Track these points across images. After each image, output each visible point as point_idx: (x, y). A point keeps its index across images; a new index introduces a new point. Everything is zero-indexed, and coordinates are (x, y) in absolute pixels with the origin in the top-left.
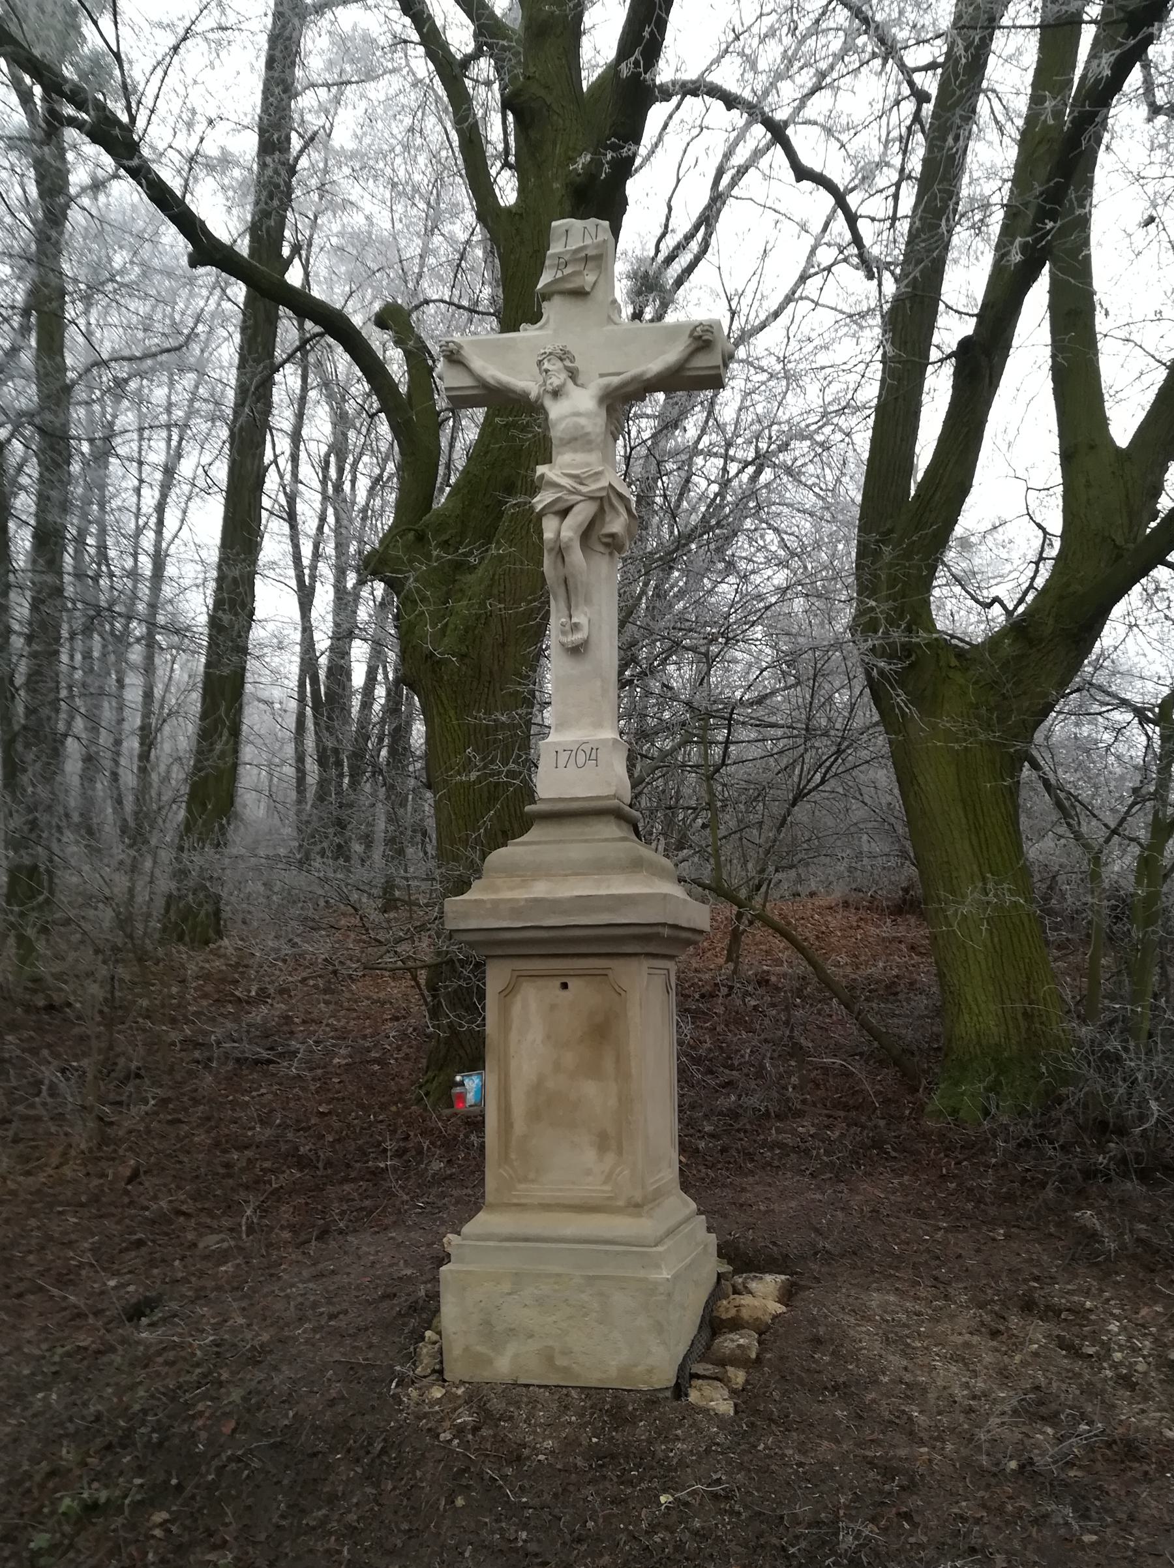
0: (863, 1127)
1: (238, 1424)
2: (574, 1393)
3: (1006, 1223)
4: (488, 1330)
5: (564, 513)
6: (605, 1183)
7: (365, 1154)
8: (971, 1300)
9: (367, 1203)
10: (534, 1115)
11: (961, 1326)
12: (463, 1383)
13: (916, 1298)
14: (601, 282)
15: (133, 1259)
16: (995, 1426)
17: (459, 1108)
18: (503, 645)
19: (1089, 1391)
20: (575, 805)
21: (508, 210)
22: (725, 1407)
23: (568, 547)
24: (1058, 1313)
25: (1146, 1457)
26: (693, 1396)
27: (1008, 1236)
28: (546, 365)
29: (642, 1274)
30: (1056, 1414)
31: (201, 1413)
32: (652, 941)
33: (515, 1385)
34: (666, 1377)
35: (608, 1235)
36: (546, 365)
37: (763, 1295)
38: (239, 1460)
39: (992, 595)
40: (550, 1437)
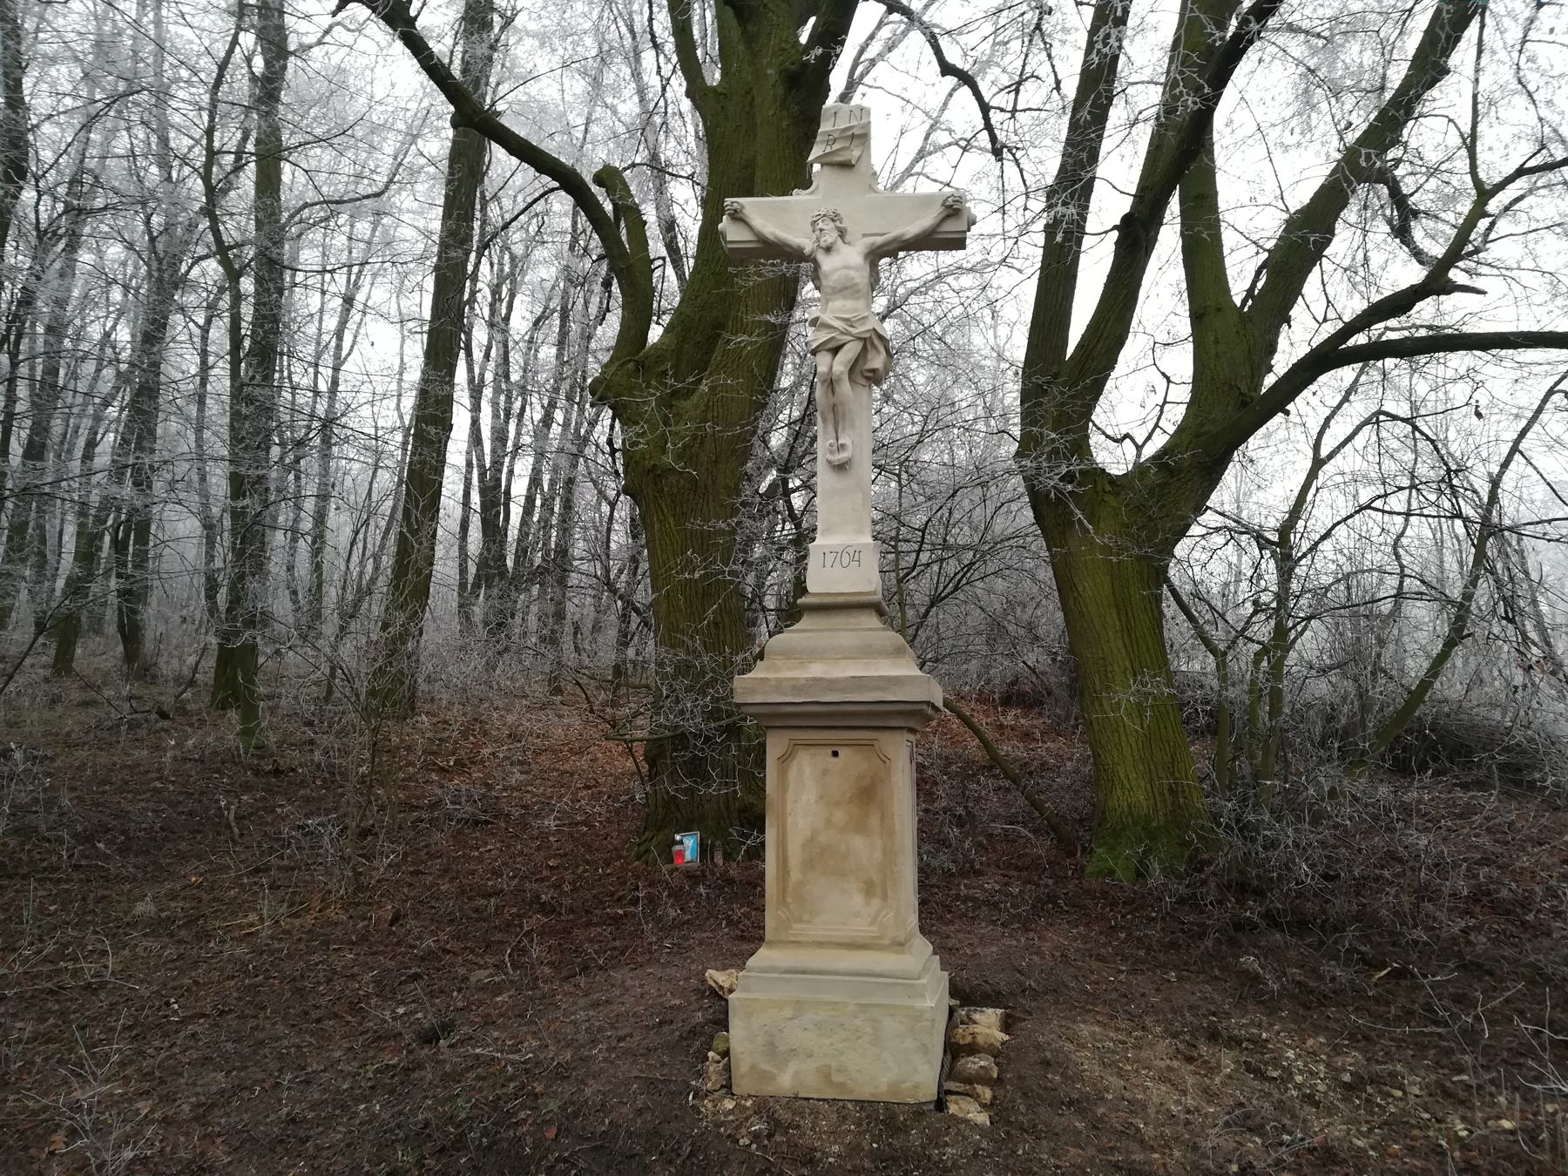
0: (1038, 886)
1: (559, 1130)
2: (850, 1106)
3: (1176, 968)
4: (771, 1048)
5: (835, 351)
6: (871, 924)
7: (601, 902)
8: (1165, 1031)
9: (617, 943)
10: (809, 864)
11: (1160, 1052)
12: (750, 1096)
13: (1117, 1030)
14: (863, 159)
15: (417, 988)
16: (1213, 1139)
17: (677, 863)
18: (716, 462)
19: (1280, 1106)
20: (841, 599)
21: (714, 89)
22: (982, 1118)
23: (839, 380)
24: (1239, 1043)
25: (1344, 1161)
26: (953, 1109)
27: (1179, 979)
28: (821, 225)
29: (908, 1003)
30: (1262, 1126)
31: (524, 1121)
32: (911, 717)
33: (796, 1098)
34: (929, 1092)
35: (878, 969)
36: (821, 225)
37: (987, 1024)
38: (565, 1160)
39: (1124, 432)
40: (835, 1143)
